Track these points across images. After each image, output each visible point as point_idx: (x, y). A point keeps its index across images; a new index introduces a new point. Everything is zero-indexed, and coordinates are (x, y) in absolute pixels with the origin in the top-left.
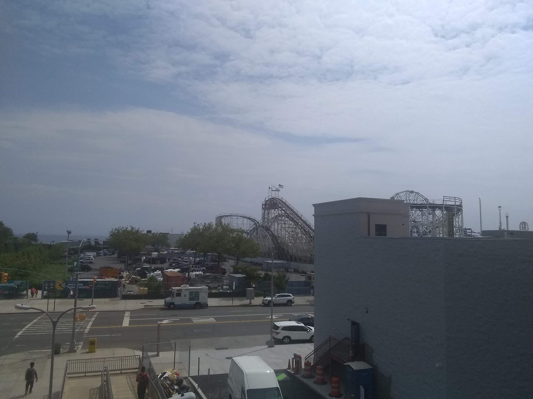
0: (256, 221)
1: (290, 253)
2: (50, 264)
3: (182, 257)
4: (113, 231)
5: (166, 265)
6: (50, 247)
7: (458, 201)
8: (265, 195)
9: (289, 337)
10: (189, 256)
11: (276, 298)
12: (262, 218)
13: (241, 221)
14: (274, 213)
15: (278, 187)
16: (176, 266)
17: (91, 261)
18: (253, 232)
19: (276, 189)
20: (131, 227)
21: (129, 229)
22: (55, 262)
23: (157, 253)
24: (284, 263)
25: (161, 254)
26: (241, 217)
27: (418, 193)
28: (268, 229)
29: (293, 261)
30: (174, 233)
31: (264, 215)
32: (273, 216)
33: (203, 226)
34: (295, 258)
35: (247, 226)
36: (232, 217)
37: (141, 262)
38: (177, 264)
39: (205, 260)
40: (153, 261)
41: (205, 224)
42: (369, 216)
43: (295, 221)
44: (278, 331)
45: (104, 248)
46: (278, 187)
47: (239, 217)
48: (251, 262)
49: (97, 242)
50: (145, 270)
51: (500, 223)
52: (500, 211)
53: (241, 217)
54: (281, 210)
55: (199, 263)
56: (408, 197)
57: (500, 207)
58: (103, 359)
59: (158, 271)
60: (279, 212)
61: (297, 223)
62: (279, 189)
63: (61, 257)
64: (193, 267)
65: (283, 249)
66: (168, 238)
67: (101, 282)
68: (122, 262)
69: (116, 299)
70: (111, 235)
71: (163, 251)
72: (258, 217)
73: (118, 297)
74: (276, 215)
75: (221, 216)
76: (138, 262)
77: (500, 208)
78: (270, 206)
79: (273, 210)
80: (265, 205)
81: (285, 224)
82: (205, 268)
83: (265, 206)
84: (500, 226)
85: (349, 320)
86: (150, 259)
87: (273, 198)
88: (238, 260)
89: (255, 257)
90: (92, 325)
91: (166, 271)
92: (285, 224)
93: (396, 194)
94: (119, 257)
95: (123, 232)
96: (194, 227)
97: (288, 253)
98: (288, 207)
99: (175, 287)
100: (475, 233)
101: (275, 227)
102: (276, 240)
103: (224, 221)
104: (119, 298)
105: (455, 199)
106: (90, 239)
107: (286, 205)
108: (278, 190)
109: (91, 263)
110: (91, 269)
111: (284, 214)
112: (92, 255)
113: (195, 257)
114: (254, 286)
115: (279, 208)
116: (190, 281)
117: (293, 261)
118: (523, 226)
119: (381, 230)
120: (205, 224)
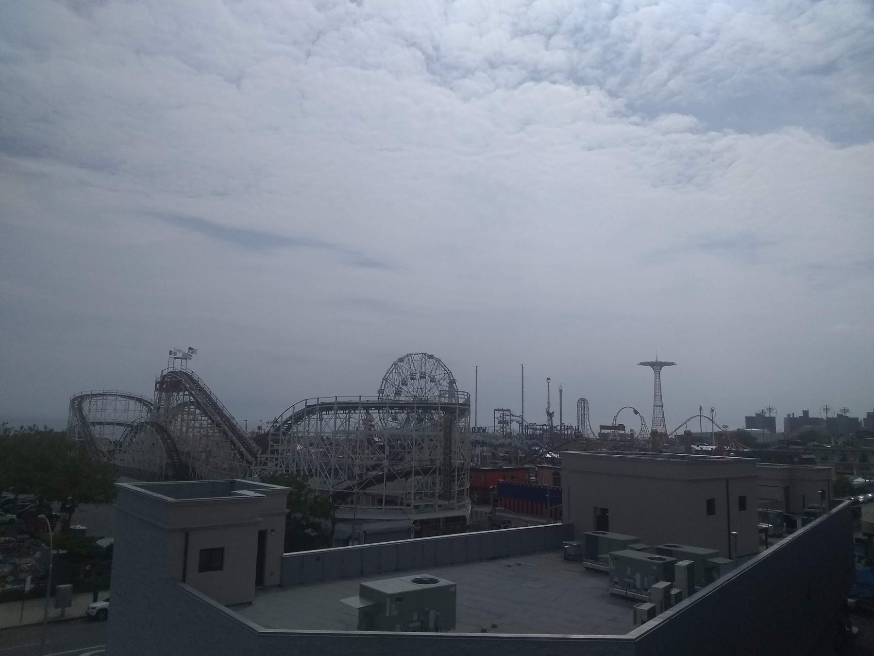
7: (463, 396)
8: (162, 365)
14: (180, 397)
15: (186, 351)
26: (124, 396)
27: (438, 360)
28: (161, 429)
46: (186, 351)
47: (119, 398)
51: (549, 403)
53: (124, 396)
57: (548, 379)
75: (84, 396)
77: (548, 381)
83: (161, 386)
84: (549, 407)
87: (175, 372)
100: (515, 416)
101: (176, 427)
107: (198, 386)
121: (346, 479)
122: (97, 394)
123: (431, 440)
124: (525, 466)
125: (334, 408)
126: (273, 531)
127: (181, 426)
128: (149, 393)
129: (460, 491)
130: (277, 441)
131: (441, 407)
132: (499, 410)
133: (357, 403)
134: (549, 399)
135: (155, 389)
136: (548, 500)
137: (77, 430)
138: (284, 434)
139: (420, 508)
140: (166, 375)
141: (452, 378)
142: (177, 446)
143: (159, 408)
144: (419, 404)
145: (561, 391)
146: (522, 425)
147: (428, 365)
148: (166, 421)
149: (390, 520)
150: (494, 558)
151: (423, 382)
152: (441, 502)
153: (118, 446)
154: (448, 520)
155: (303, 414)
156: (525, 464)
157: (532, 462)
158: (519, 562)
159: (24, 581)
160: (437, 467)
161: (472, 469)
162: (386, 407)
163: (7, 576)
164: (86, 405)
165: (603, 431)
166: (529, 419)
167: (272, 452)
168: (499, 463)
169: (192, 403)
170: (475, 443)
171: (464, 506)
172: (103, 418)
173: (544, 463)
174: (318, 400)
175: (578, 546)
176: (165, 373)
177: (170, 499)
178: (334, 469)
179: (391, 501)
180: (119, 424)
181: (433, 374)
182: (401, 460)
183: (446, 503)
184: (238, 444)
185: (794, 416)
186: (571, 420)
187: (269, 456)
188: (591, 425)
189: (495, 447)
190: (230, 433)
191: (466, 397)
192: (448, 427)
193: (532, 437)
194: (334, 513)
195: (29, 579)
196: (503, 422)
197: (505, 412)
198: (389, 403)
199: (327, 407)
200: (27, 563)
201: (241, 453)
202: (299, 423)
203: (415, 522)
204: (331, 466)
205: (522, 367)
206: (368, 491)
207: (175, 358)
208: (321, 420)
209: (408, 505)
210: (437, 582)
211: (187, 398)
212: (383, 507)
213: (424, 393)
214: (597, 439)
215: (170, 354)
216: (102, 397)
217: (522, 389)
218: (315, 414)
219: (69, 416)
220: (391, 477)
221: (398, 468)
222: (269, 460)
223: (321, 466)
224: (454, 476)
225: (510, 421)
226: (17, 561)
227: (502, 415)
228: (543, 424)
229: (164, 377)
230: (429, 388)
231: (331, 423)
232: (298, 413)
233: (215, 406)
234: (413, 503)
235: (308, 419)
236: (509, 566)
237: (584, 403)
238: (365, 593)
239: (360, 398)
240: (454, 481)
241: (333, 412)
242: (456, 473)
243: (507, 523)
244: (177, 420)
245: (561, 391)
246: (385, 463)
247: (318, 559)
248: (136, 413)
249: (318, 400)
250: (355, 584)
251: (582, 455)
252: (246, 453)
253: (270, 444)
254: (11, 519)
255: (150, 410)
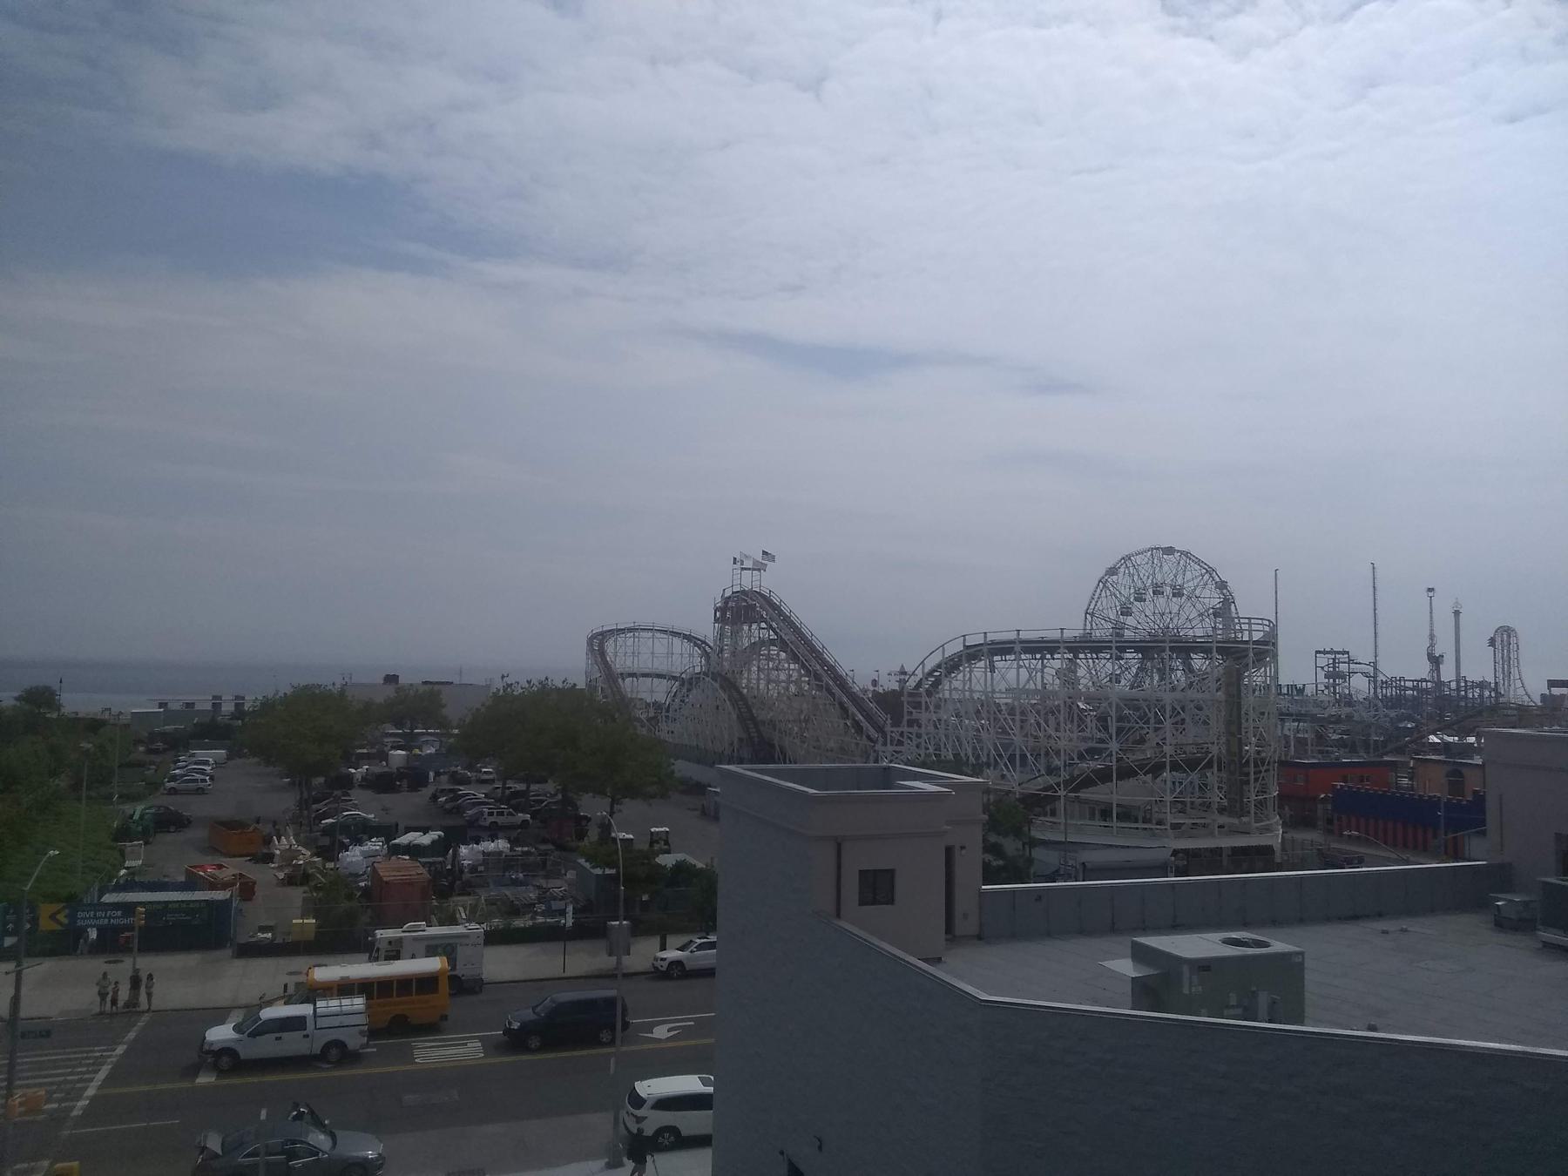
7: (1260, 627)
8: (723, 581)
9: (673, 1130)
11: (691, 952)
15: (759, 557)
17: (201, 785)
19: (754, 564)
23: (404, 753)
26: (665, 632)
27: (1186, 554)
28: (729, 684)
30: (465, 681)
33: (522, 688)
36: (637, 634)
41: (529, 682)
42: (839, 845)
44: (639, 1113)
46: (759, 557)
47: (658, 635)
51: (1432, 637)
52: (1431, 603)
53: (665, 632)
56: (1159, 565)
57: (1430, 590)
60: (761, 636)
64: (491, 814)
67: (177, 905)
69: (218, 954)
77: (1431, 594)
84: (1432, 645)
85: (782, 1153)
87: (743, 592)
90: (110, 1080)
93: (1123, 558)
100: (1360, 663)
101: (752, 679)
105: (1250, 624)
106: (220, 698)
107: (781, 613)
118: (1502, 638)
120: (529, 682)
121: (1043, 772)
123: (1200, 708)
124: (1386, 758)
125: (1016, 649)
126: (963, 848)
127: (758, 679)
128: (706, 628)
129: (1260, 802)
130: (917, 706)
131: (1217, 647)
132: (1325, 652)
133: (1058, 642)
134: (1432, 630)
136: (1442, 821)
137: (600, 684)
138: (929, 693)
139: (1183, 828)
140: (730, 597)
142: (754, 711)
143: (722, 651)
145: (1457, 613)
146: (1375, 682)
147: (1166, 568)
148: (734, 671)
149: (1128, 847)
150: (1355, 918)
151: (1161, 601)
152: (1223, 820)
153: (664, 711)
154: (1236, 851)
155: (960, 660)
156: (1386, 754)
157: (1400, 751)
158: (1404, 927)
159: (563, 913)
160: (1213, 756)
161: (1282, 763)
162: (1110, 648)
163: (534, 904)
164: (610, 647)
165: (1556, 691)
166: (1389, 670)
167: (911, 723)
168: (1333, 752)
169: (772, 642)
170: (1283, 716)
171: (1268, 829)
172: (636, 666)
173: (1425, 753)
174: (985, 637)
175: (1526, 904)
176: (729, 593)
177: (812, 791)
178: (1020, 755)
179: (1126, 814)
180: (659, 676)
181: (1180, 581)
182: (1142, 741)
183: (1236, 821)
184: (852, 709)
185: (132, 959)
186: (1479, 667)
187: (906, 729)
188: (1523, 678)
189: (1323, 722)
190: (836, 690)
191: (1267, 629)
192: (1233, 685)
193: (1395, 702)
194: (1029, 830)
195: (570, 909)
196: (1334, 675)
197: (1338, 656)
198: (1117, 642)
199: (1002, 648)
200: (558, 886)
201: (857, 725)
202: (953, 675)
203: (1175, 853)
204: (1014, 750)
205: (1374, 568)
206: (1083, 794)
207: (742, 569)
208: (992, 671)
209: (1160, 823)
210: (1269, 946)
211: (765, 634)
212: (1115, 823)
213: (1168, 620)
214: (1536, 706)
215: (735, 563)
217: (1373, 612)
218: (981, 660)
219: (587, 664)
220: (1126, 773)
221: (1134, 757)
222: (905, 737)
223: (996, 749)
224: (1248, 774)
225: (1349, 673)
226: (543, 882)
227: (1331, 661)
228: (1419, 678)
229: (726, 600)
230: (1175, 610)
231: (1011, 674)
232: (951, 659)
233: (812, 649)
234: (1170, 819)
235: (968, 669)
236: (1385, 932)
237: (1509, 636)
238: (1141, 955)
239: (1062, 633)
240: (1248, 782)
241: (1013, 657)
242: (1252, 770)
243: (1356, 862)
244: (749, 670)
245: (1457, 613)
246: (1114, 746)
247: (1039, 898)
248: (685, 660)
249: (985, 637)
250: (1123, 943)
251: (1529, 735)
252: (865, 724)
253: (905, 710)
254: (523, 821)
255: (706, 655)
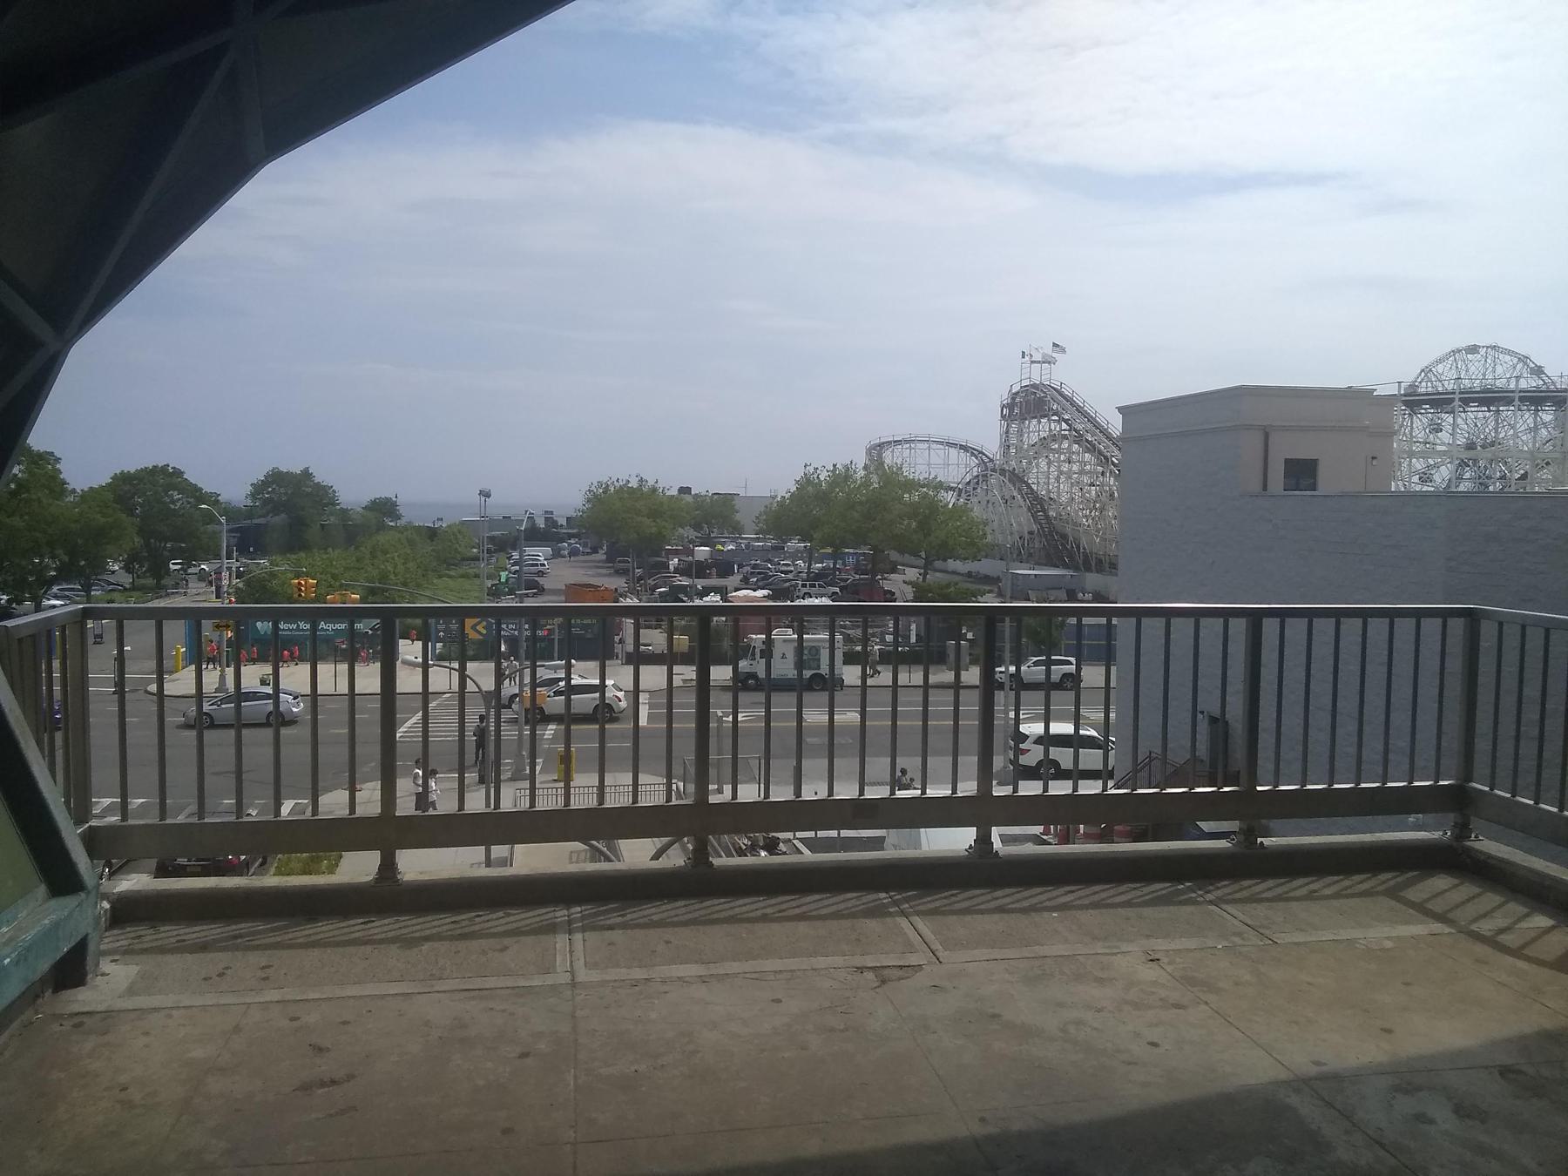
0: (984, 455)
1: (1084, 548)
2: (440, 577)
3: (776, 560)
4: (593, 488)
5: (735, 580)
6: (432, 533)
8: (1011, 378)
10: (794, 556)
12: (1000, 447)
13: (939, 456)
14: (1037, 429)
15: (1049, 350)
16: (760, 584)
17: (540, 568)
18: (974, 489)
19: (1043, 357)
20: (637, 479)
21: (634, 484)
22: (452, 573)
23: (707, 548)
24: (1063, 576)
25: (719, 550)
26: (941, 443)
28: (1017, 478)
29: (1093, 568)
31: (1007, 436)
32: (1034, 438)
34: (1100, 562)
35: (955, 469)
36: (913, 446)
37: (670, 573)
38: (763, 579)
39: (838, 566)
40: (700, 570)
42: (1267, 436)
43: (1100, 453)
45: (571, 536)
46: (1049, 350)
47: (934, 446)
48: (969, 574)
49: (550, 521)
50: (681, 593)
53: (941, 443)
54: (1059, 421)
55: (820, 576)
58: (554, 790)
59: (713, 594)
60: (1053, 428)
61: (1106, 458)
62: (1054, 355)
63: (464, 559)
64: (804, 586)
65: (1064, 537)
66: (737, 507)
68: (619, 573)
70: (589, 501)
71: (723, 544)
72: (992, 446)
73: (617, 658)
74: (1043, 435)
75: (883, 443)
76: (659, 573)
78: (1024, 411)
79: (1034, 422)
80: (1011, 406)
81: (1069, 463)
82: (837, 590)
86: (690, 564)
87: (1034, 386)
88: (927, 567)
89: (975, 558)
91: (734, 594)
92: (1069, 463)
94: (610, 558)
95: (617, 492)
96: (805, 474)
97: (1078, 547)
98: (1079, 410)
99: (756, 634)
101: (1042, 475)
102: (1044, 510)
103: (889, 458)
104: (620, 662)
107: (1073, 404)
108: (1048, 361)
109: (540, 574)
110: (544, 589)
111: (1067, 432)
112: (540, 554)
113: (810, 560)
114: (970, 636)
115: (1053, 415)
116: (800, 618)
117: (1093, 568)
119: (1302, 473)
120: (834, 466)
122: (901, 441)
128: (989, 437)
135: (1002, 417)
141: (1533, 366)
144: (1524, 392)
207: (1032, 362)
215: (1023, 357)
216: (908, 445)
